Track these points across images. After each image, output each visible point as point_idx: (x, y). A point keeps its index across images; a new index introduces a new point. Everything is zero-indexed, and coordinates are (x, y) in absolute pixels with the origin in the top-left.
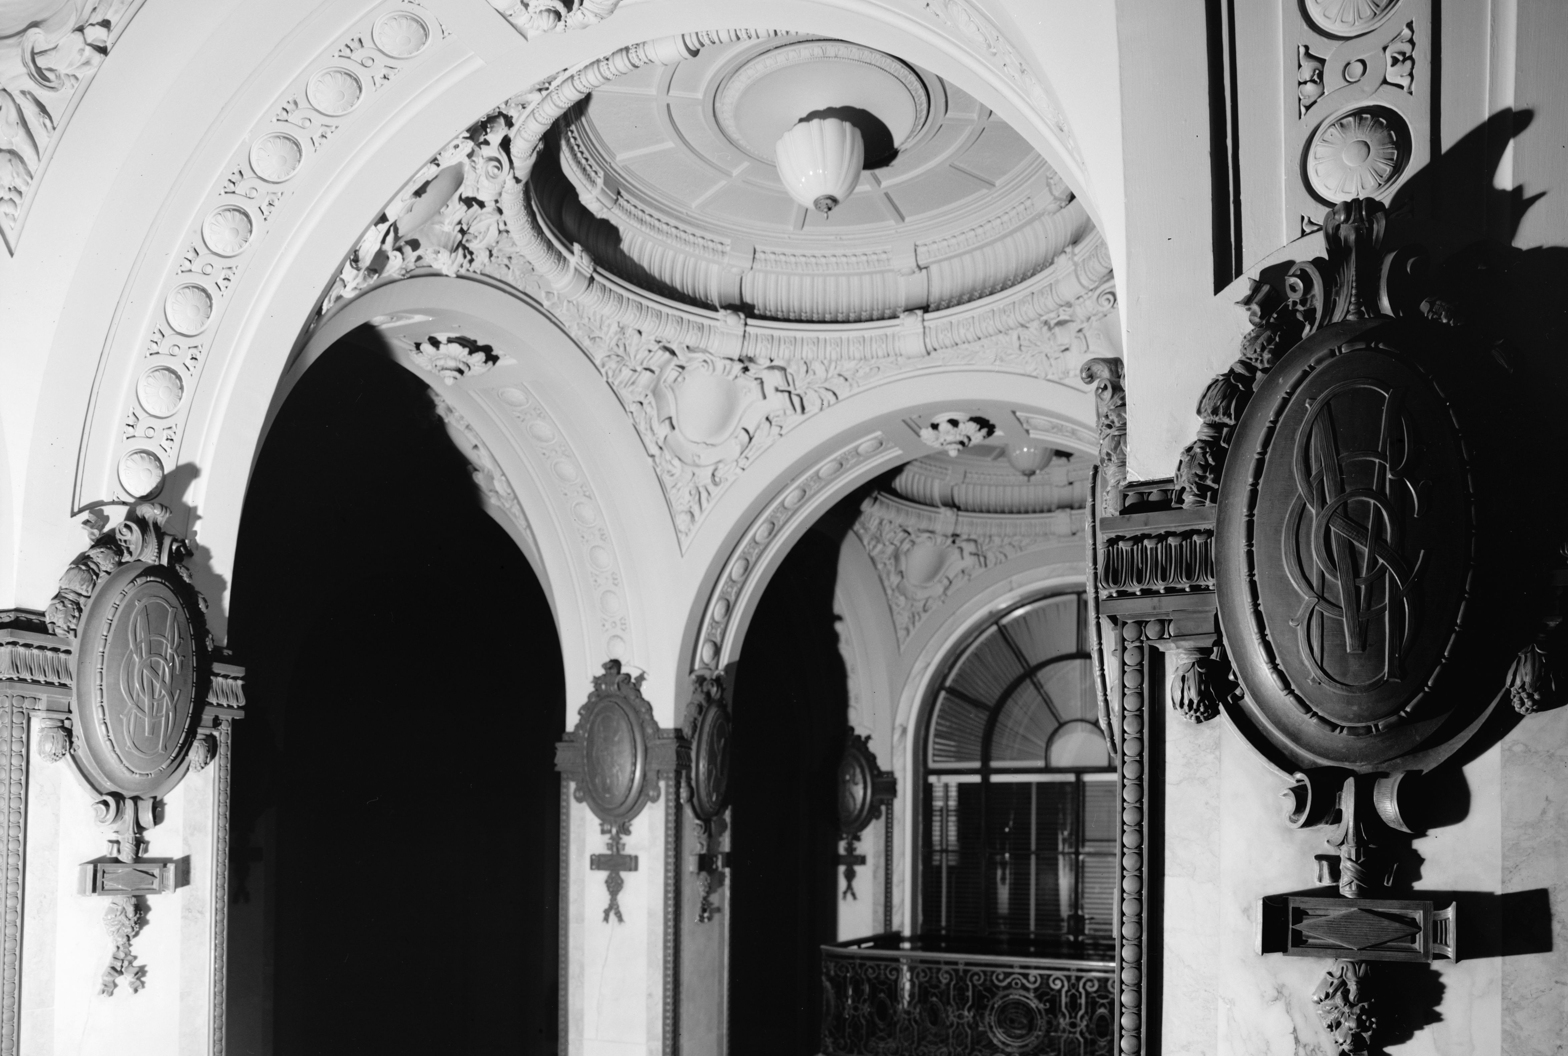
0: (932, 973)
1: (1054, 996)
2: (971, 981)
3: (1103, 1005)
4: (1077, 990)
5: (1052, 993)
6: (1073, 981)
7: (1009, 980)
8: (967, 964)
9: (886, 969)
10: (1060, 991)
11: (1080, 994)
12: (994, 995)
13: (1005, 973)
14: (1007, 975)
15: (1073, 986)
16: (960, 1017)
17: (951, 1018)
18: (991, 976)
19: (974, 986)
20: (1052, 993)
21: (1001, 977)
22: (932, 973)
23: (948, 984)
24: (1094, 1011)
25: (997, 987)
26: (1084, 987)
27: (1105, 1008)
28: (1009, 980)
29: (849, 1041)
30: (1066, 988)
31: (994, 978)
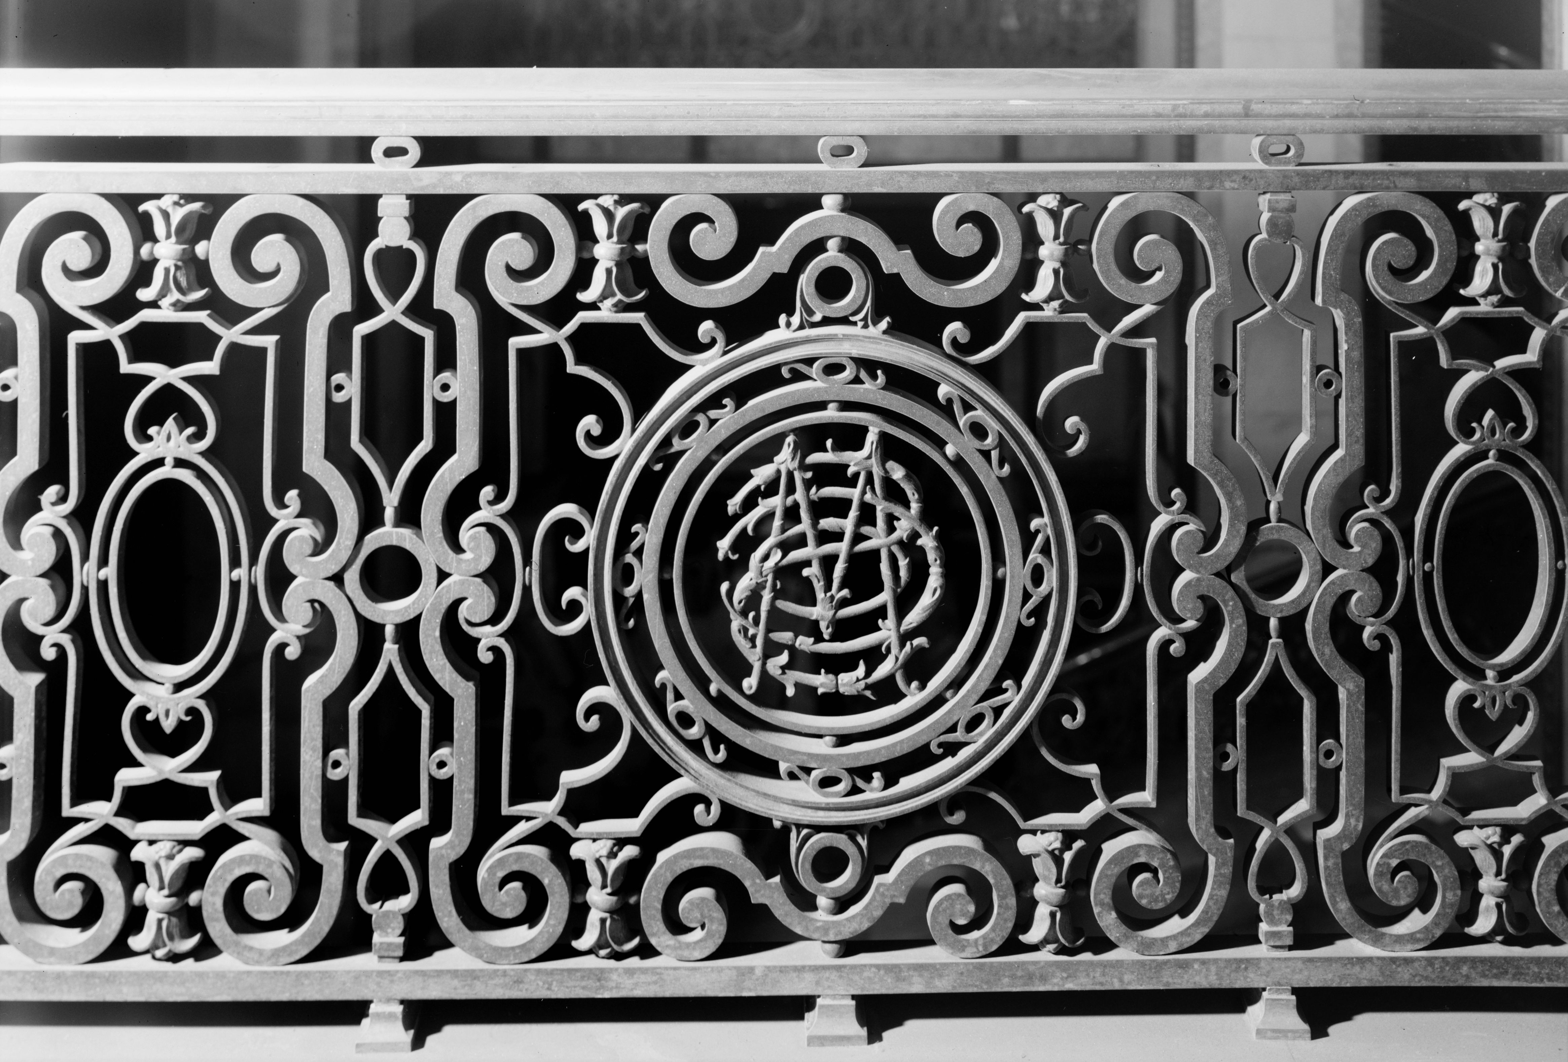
0: (143, 230)
1: (244, 359)
2: (471, 278)
3: (168, 404)
4: (423, 308)
5: (231, 335)
6: (393, 230)
7: (771, 259)
8: (438, 150)
9: (200, 227)
10: (289, 323)
11: (444, 326)
12: (648, 377)
13: (744, 206)
14: (761, 217)
15: (396, 267)
16: (392, 574)
17: (309, 579)
18: (637, 229)
19: (496, 325)
20: (231, 335)
21: (712, 242)
22: (143, 230)
23: (289, 323)
24: (107, 454)
25: (681, 323)
26: (471, 278)
27: (190, 416)
28: (771, 259)
29: (331, 856)
30: (337, 299)
31: (656, 247)
